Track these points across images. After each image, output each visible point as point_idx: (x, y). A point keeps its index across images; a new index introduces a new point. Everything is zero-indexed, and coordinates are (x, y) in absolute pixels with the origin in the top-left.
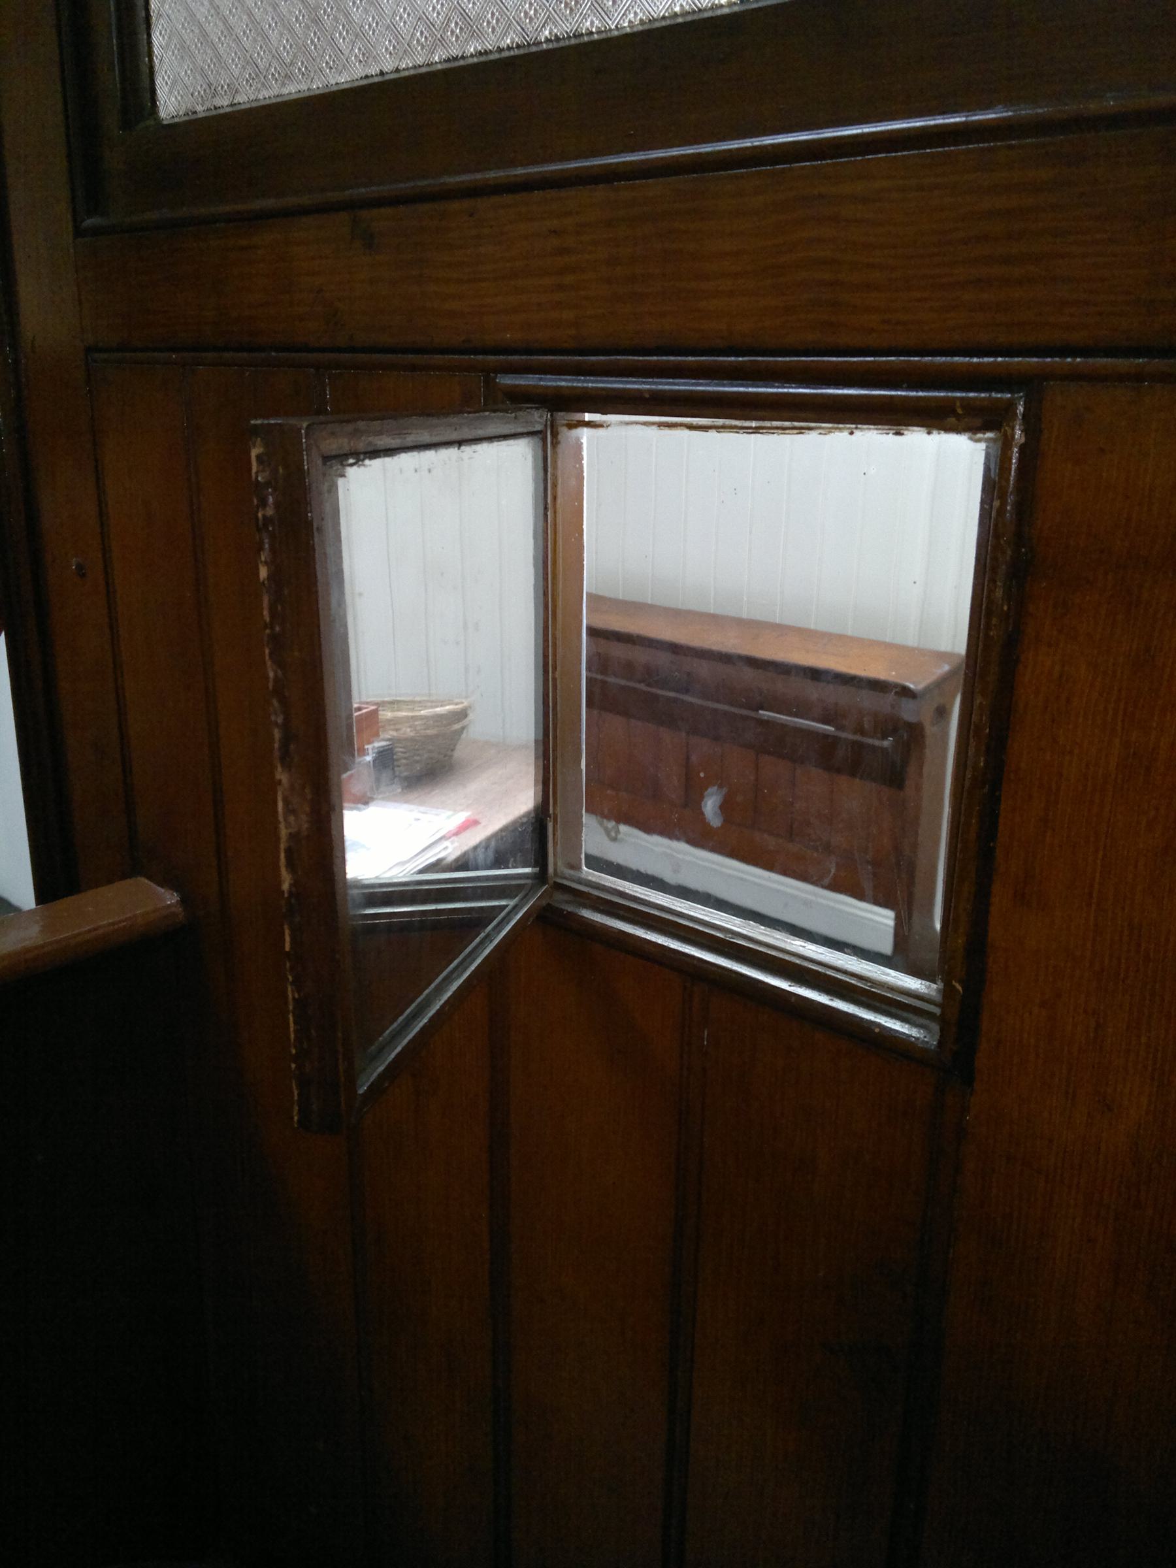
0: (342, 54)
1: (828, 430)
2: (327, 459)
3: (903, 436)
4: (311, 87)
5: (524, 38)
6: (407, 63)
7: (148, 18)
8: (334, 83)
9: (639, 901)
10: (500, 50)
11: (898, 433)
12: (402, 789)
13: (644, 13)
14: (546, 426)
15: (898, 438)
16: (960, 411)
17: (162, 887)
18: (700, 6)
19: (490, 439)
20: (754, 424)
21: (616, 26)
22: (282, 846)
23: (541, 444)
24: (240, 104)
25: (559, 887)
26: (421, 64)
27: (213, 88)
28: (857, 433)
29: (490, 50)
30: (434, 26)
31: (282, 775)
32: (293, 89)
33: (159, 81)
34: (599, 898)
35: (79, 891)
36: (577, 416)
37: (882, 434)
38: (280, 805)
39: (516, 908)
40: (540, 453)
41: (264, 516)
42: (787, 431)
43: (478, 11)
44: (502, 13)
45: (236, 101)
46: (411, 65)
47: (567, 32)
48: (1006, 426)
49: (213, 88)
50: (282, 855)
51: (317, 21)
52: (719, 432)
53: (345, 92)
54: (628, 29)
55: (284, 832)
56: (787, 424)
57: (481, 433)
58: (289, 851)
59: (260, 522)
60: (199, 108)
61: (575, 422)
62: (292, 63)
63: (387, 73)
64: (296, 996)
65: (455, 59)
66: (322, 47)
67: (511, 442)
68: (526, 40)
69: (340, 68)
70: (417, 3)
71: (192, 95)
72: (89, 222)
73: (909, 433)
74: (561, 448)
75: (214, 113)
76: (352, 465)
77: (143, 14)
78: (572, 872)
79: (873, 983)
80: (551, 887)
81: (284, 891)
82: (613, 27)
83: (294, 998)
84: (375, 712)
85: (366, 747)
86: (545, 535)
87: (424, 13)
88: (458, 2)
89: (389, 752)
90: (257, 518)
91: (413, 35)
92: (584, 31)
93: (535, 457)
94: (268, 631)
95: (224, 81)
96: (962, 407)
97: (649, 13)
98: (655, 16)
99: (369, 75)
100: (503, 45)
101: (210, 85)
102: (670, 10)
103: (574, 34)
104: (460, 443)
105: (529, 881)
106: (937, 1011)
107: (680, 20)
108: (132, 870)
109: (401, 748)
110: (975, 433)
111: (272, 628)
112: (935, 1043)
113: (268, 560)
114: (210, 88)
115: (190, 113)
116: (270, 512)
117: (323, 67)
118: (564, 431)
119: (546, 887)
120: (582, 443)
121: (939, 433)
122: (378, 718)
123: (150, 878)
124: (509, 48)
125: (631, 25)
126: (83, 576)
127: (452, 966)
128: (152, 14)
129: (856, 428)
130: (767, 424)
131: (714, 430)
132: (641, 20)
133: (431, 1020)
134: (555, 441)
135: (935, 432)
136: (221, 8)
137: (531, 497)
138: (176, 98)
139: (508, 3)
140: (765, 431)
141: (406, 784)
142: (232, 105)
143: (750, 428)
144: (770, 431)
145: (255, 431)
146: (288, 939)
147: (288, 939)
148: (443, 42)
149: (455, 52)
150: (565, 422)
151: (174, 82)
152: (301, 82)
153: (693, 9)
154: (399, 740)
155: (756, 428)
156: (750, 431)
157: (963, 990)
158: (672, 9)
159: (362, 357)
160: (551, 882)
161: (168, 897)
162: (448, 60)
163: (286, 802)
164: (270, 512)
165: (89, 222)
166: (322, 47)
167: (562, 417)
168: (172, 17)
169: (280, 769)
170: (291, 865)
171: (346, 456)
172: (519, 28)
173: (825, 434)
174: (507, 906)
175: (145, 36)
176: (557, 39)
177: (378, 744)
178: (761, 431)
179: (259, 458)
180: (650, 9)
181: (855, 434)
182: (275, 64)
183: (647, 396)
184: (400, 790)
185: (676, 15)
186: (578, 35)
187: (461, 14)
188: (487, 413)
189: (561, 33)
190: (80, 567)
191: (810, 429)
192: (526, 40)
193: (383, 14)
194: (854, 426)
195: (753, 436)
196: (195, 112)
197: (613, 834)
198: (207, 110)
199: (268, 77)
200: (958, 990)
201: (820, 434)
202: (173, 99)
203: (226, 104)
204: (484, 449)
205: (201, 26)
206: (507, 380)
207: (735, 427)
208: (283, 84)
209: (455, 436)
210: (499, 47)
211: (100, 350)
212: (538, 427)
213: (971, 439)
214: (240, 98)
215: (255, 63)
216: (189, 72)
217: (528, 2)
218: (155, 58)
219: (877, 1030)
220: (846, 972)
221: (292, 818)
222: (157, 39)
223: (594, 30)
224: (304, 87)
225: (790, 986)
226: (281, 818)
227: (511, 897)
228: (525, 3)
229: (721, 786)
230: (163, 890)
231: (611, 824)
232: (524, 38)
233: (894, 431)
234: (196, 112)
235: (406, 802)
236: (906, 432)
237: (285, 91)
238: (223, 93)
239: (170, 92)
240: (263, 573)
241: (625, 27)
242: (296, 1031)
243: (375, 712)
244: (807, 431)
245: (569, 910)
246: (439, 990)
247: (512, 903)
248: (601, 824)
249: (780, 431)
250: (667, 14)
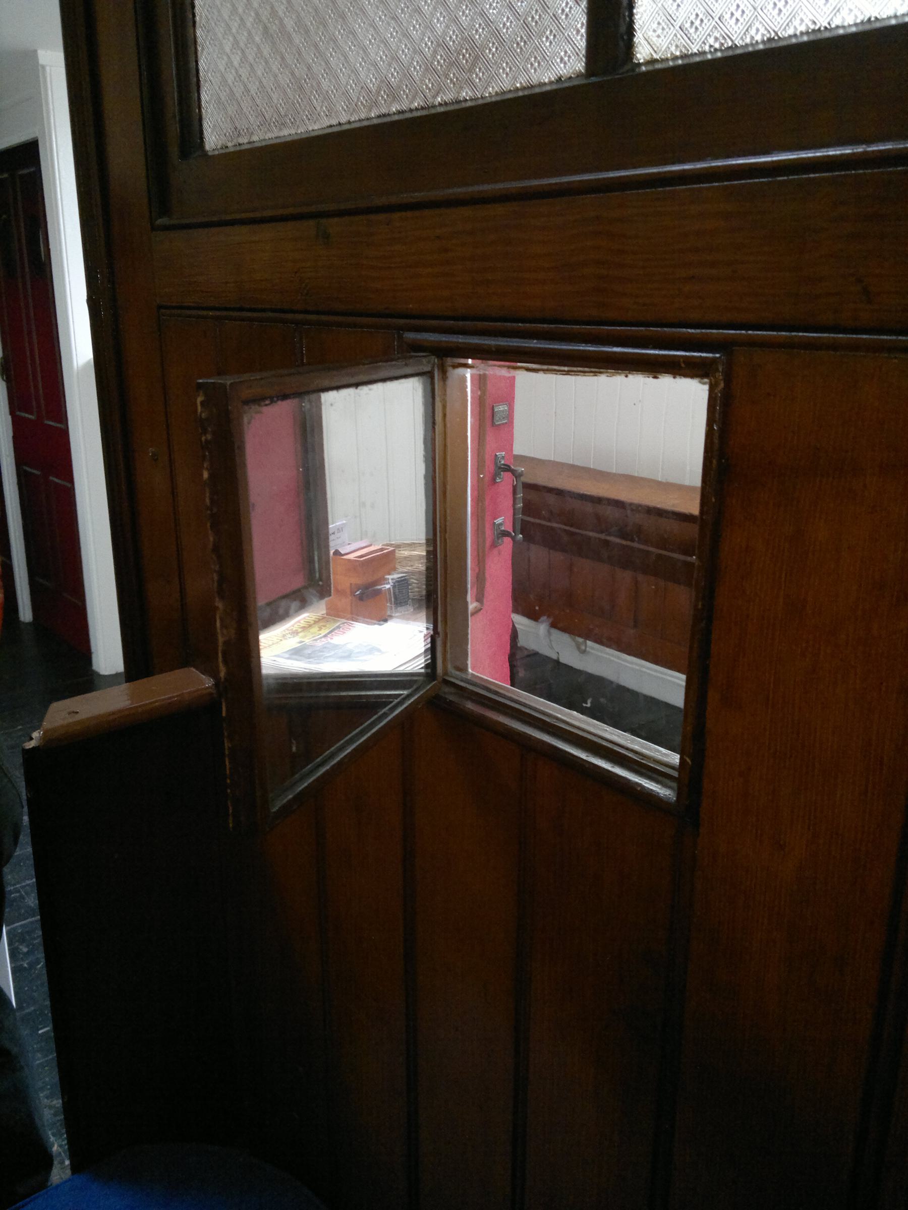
0: (316, 110)
1: (612, 374)
2: (247, 402)
3: (658, 379)
4: (297, 132)
5: (426, 103)
6: (355, 118)
7: (198, 81)
8: (311, 130)
9: (499, 695)
10: (411, 110)
11: (655, 377)
12: (414, 609)
13: (498, 88)
14: (433, 367)
15: (655, 380)
16: (683, 365)
17: (203, 674)
18: (532, 83)
19: (384, 380)
20: (566, 369)
21: (481, 96)
22: (220, 648)
23: (429, 380)
24: (254, 142)
25: (446, 682)
26: (363, 118)
27: (238, 131)
28: (630, 376)
29: (405, 110)
30: (371, 93)
31: (219, 604)
32: (288, 132)
33: (205, 125)
34: (472, 691)
35: (153, 675)
36: (462, 361)
37: (645, 377)
38: (218, 624)
39: (408, 697)
40: (429, 388)
41: (206, 440)
42: (586, 374)
43: (525, 9)
44: (411, 84)
45: (251, 140)
46: (357, 119)
47: (451, 99)
48: (712, 376)
49: (238, 131)
50: (220, 655)
51: (301, 88)
52: (545, 373)
53: (318, 138)
54: (489, 98)
55: (221, 640)
56: (586, 369)
57: (375, 377)
58: (224, 653)
59: (204, 444)
60: (230, 144)
61: (456, 364)
62: (286, 115)
63: (343, 124)
64: (230, 745)
65: (384, 115)
66: (348, 74)
67: (403, 381)
68: (427, 104)
69: (315, 119)
70: (476, 2)
71: (225, 135)
72: (159, 222)
73: (662, 377)
74: (449, 382)
75: (238, 148)
76: (266, 405)
77: (195, 79)
78: (458, 673)
79: (643, 756)
80: (439, 683)
81: (221, 677)
82: (479, 96)
83: (228, 747)
84: (394, 551)
85: (387, 577)
86: (433, 441)
87: (365, 84)
88: (510, 2)
89: (405, 582)
90: (201, 441)
91: (358, 98)
92: (462, 99)
93: (425, 390)
94: (209, 512)
95: (244, 126)
96: (684, 362)
97: (501, 87)
98: (505, 90)
99: (332, 125)
100: (413, 107)
101: (236, 128)
102: (514, 86)
103: (456, 101)
104: (357, 385)
105: (421, 678)
106: (675, 774)
107: (521, 94)
108: (184, 663)
109: (415, 580)
110: (702, 379)
111: (211, 510)
112: (45, 723)
113: (209, 467)
114: (236, 131)
115: (224, 147)
116: (209, 437)
117: (304, 119)
118: (450, 369)
119: (434, 683)
120: (467, 377)
121: (681, 378)
122: (395, 555)
123: (197, 669)
124: (417, 109)
125: (490, 95)
126: (156, 460)
127: (354, 733)
128: (201, 79)
129: (629, 373)
130: (575, 369)
131: (542, 372)
132: (496, 92)
133: (332, 767)
134: (444, 377)
135: (678, 377)
136: (243, 76)
137: (421, 416)
138: (215, 137)
139: (549, 2)
140: (573, 373)
141: (417, 605)
142: (249, 143)
143: (564, 371)
144: (576, 373)
145: (200, 386)
146: (224, 709)
147: (224, 709)
148: (377, 104)
149: (384, 111)
150: (451, 364)
151: (214, 126)
152: (291, 128)
153: (528, 85)
154: (413, 573)
155: (568, 371)
156: (564, 373)
157: (691, 761)
158: (515, 85)
159: (324, 318)
160: (440, 679)
161: (207, 682)
162: (379, 117)
163: (222, 620)
164: (209, 437)
165: (159, 222)
166: (348, 74)
167: (449, 361)
168: (213, 82)
169: (217, 599)
170: (225, 662)
171: (263, 399)
172: (422, 95)
173: (611, 376)
174: (402, 694)
175: (196, 95)
176: (446, 104)
177: (396, 576)
178: (571, 373)
179: (202, 403)
180: (501, 84)
181: (628, 378)
182: (275, 116)
183: (494, 349)
184: (412, 610)
185: (517, 89)
186: (458, 102)
187: (387, 85)
188: (380, 364)
189: (448, 100)
190: (154, 454)
191: (600, 373)
192: (427, 104)
193: (391, 49)
194: (628, 372)
195: (566, 376)
196: (227, 147)
197: (583, 648)
198: (234, 146)
199: (271, 124)
200: (688, 762)
201: (608, 376)
202: (214, 138)
203: (246, 141)
204: (375, 387)
205: (231, 89)
206: (410, 336)
207: (555, 370)
208: (281, 129)
209: (353, 381)
210: (410, 109)
211: (166, 308)
212: (427, 368)
213: (700, 382)
214: (255, 138)
215: (263, 115)
216: (223, 119)
217: (565, 2)
218: (202, 109)
219: (639, 789)
220: (627, 749)
221: (225, 631)
222: (204, 97)
223: (468, 98)
224: (293, 132)
225: (587, 756)
226: (219, 631)
227: (404, 688)
228: (563, 2)
229: (549, 616)
230: (204, 677)
231: (581, 640)
232: (426, 103)
233: (653, 376)
234: (227, 147)
235: (415, 620)
236: (660, 377)
237: (282, 134)
238: (244, 134)
239: (212, 132)
240: (206, 475)
241: (486, 97)
242: (230, 769)
243: (394, 551)
244: (599, 374)
245: (451, 699)
246: (341, 749)
247: (405, 692)
248: (574, 640)
249: (582, 374)
250: (512, 89)
